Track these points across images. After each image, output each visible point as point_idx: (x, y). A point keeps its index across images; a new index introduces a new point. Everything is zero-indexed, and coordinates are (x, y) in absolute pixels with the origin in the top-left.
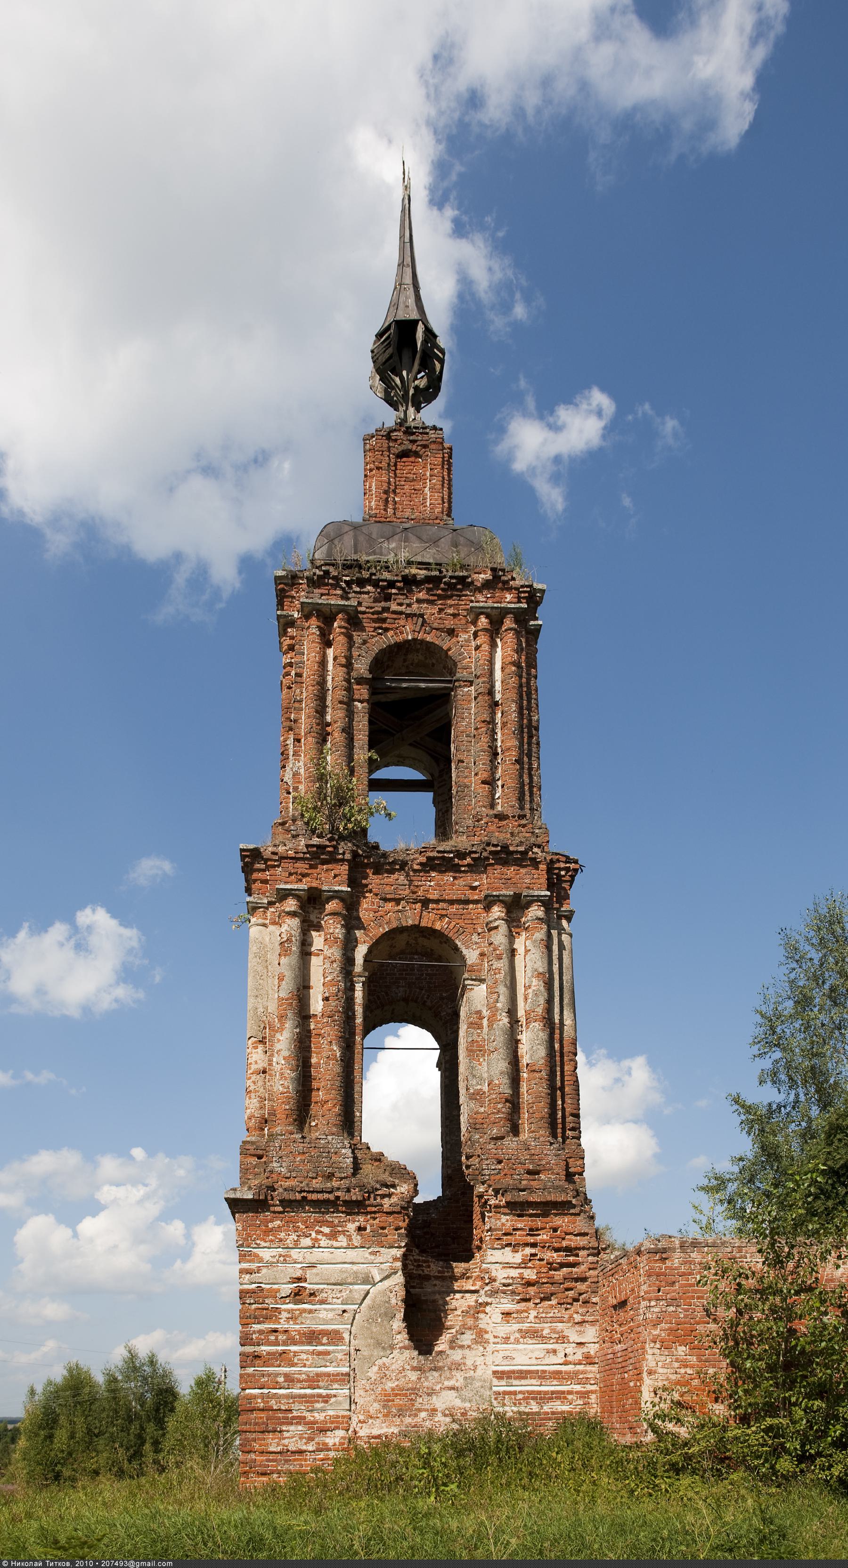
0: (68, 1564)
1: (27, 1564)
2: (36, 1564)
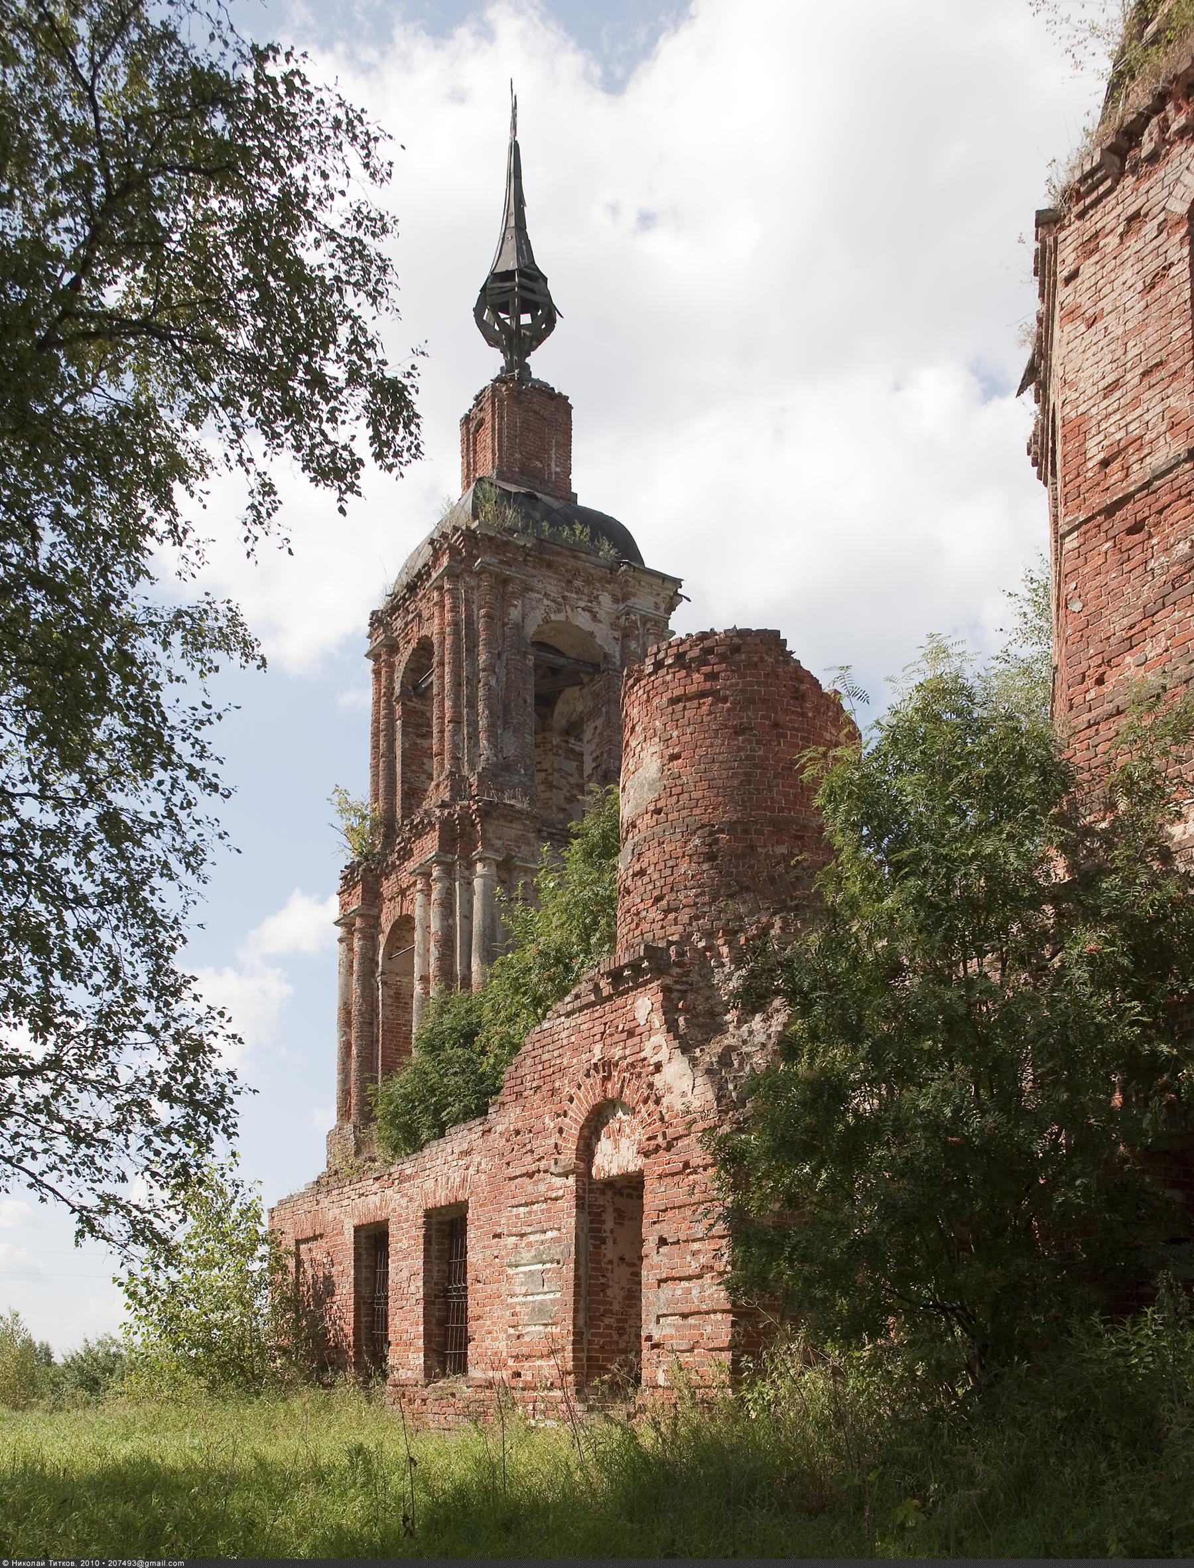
0: (73, 1564)
1: (29, 1564)
2: (39, 1564)
